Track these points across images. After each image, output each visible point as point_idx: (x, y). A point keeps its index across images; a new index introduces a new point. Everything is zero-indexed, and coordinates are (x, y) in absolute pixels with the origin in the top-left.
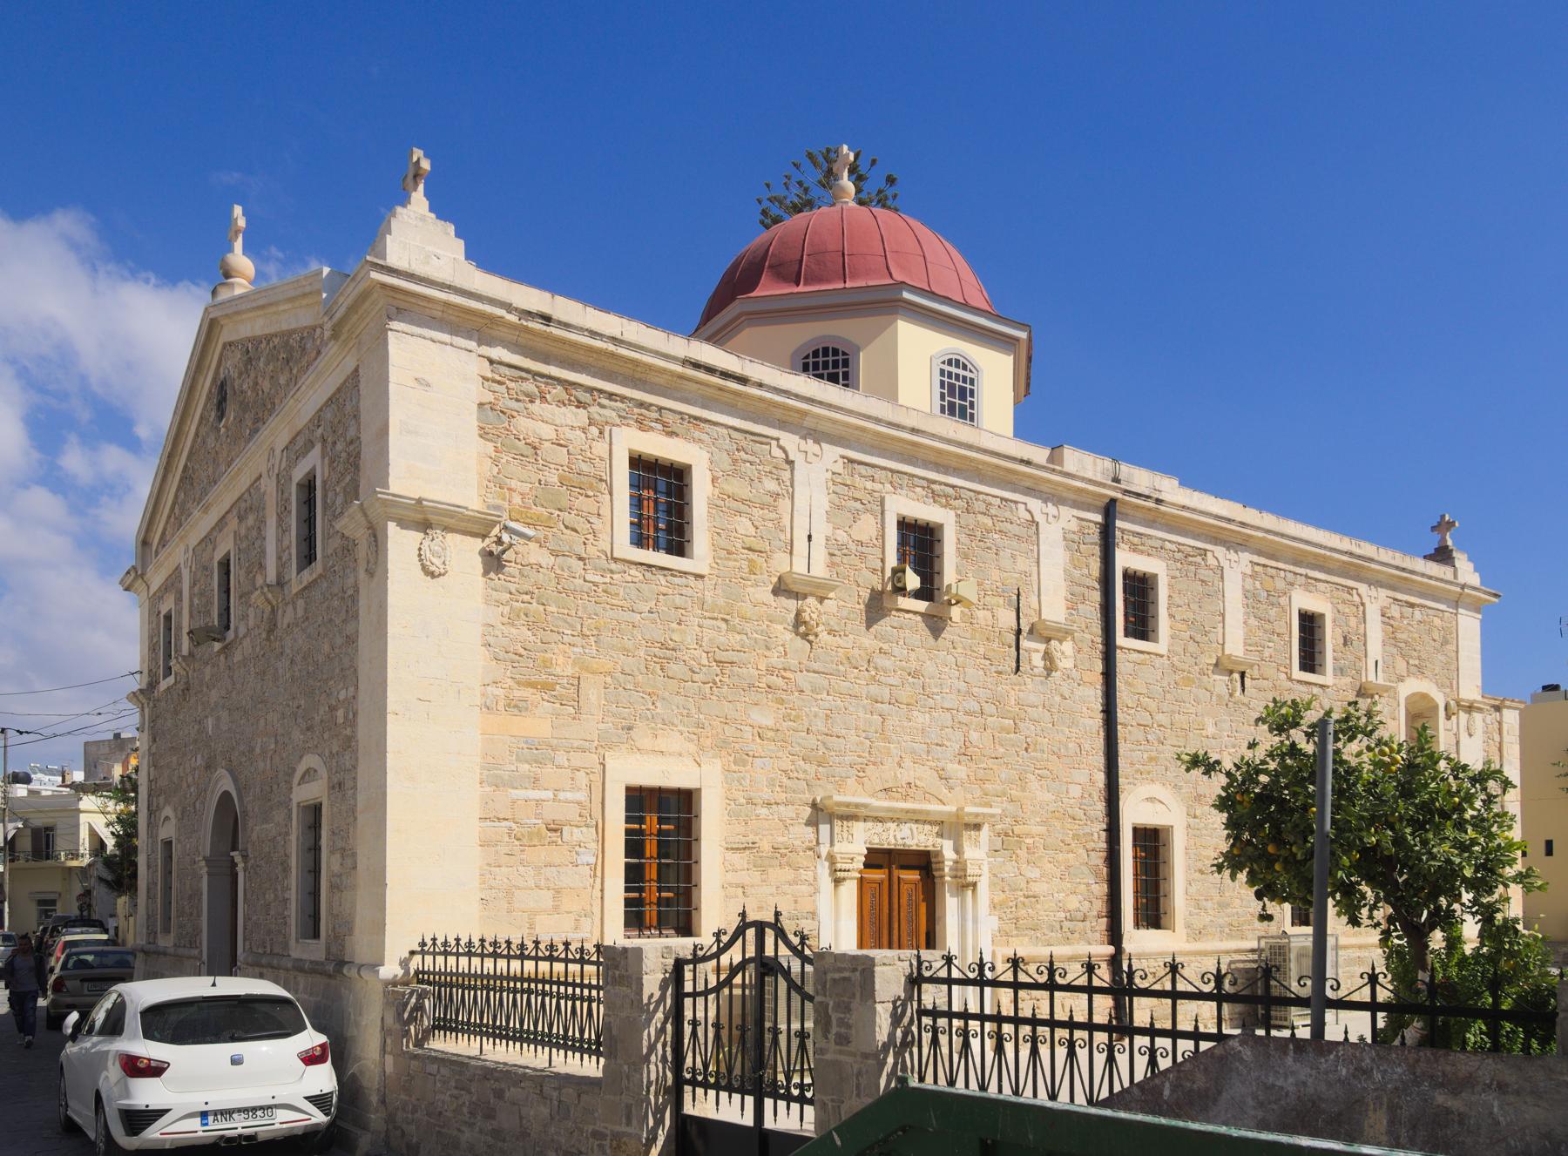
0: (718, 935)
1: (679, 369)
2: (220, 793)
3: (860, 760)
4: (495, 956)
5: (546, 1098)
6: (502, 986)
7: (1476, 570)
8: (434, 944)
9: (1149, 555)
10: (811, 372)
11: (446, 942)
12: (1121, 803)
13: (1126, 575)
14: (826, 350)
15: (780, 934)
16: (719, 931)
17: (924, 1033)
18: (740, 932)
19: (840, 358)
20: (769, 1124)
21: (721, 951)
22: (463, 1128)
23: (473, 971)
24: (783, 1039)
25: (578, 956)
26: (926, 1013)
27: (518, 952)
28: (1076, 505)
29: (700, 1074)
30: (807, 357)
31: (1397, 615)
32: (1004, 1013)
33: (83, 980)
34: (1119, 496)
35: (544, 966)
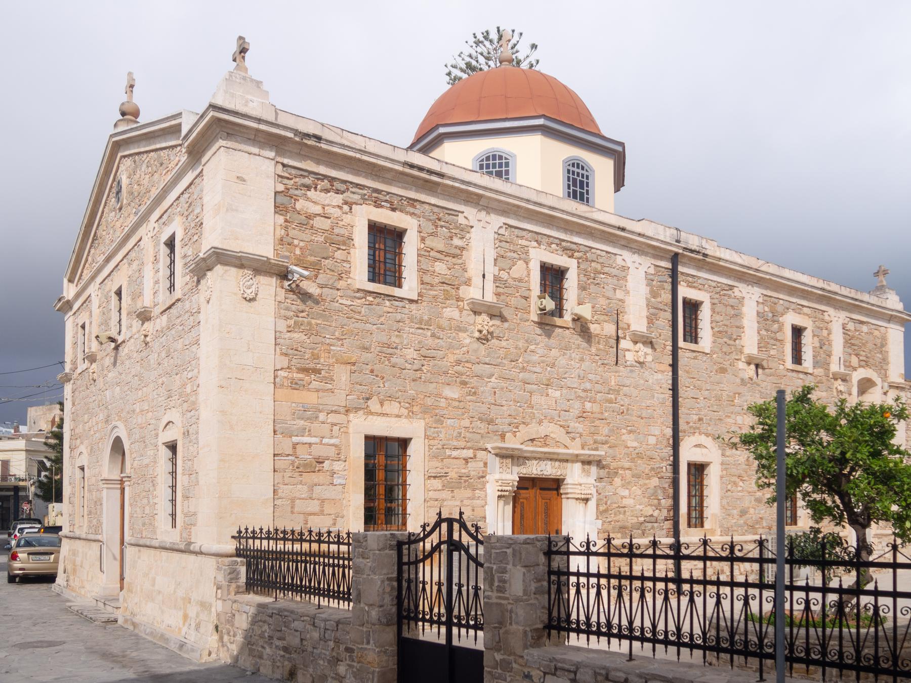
0: (424, 527)
1: (399, 168)
2: (115, 436)
3: (516, 421)
4: (285, 539)
5: (316, 627)
6: (311, 561)
7: (901, 301)
8: (247, 532)
9: (699, 289)
10: (485, 170)
11: (254, 531)
12: (680, 448)
13: (685, 300)
14: (494, 157)
15: (463, 525)
16: (425, 524)
17: (552, 586)
18: (438, 524)
19: (504, 161)
20: (455, 642)
21: (426, 536)
22: (265, 646)
23: (271, 549)
24: (428, 587)
25: (336, 540)
26: (554, 573)
27: (317, 538)
28: (655, 257)
29: (413, 612)
30: (482, 160)
31: (852, 328)
32: (581, 571)
33: (29, 554)
34: (681, 251)
35: (334, 547)
